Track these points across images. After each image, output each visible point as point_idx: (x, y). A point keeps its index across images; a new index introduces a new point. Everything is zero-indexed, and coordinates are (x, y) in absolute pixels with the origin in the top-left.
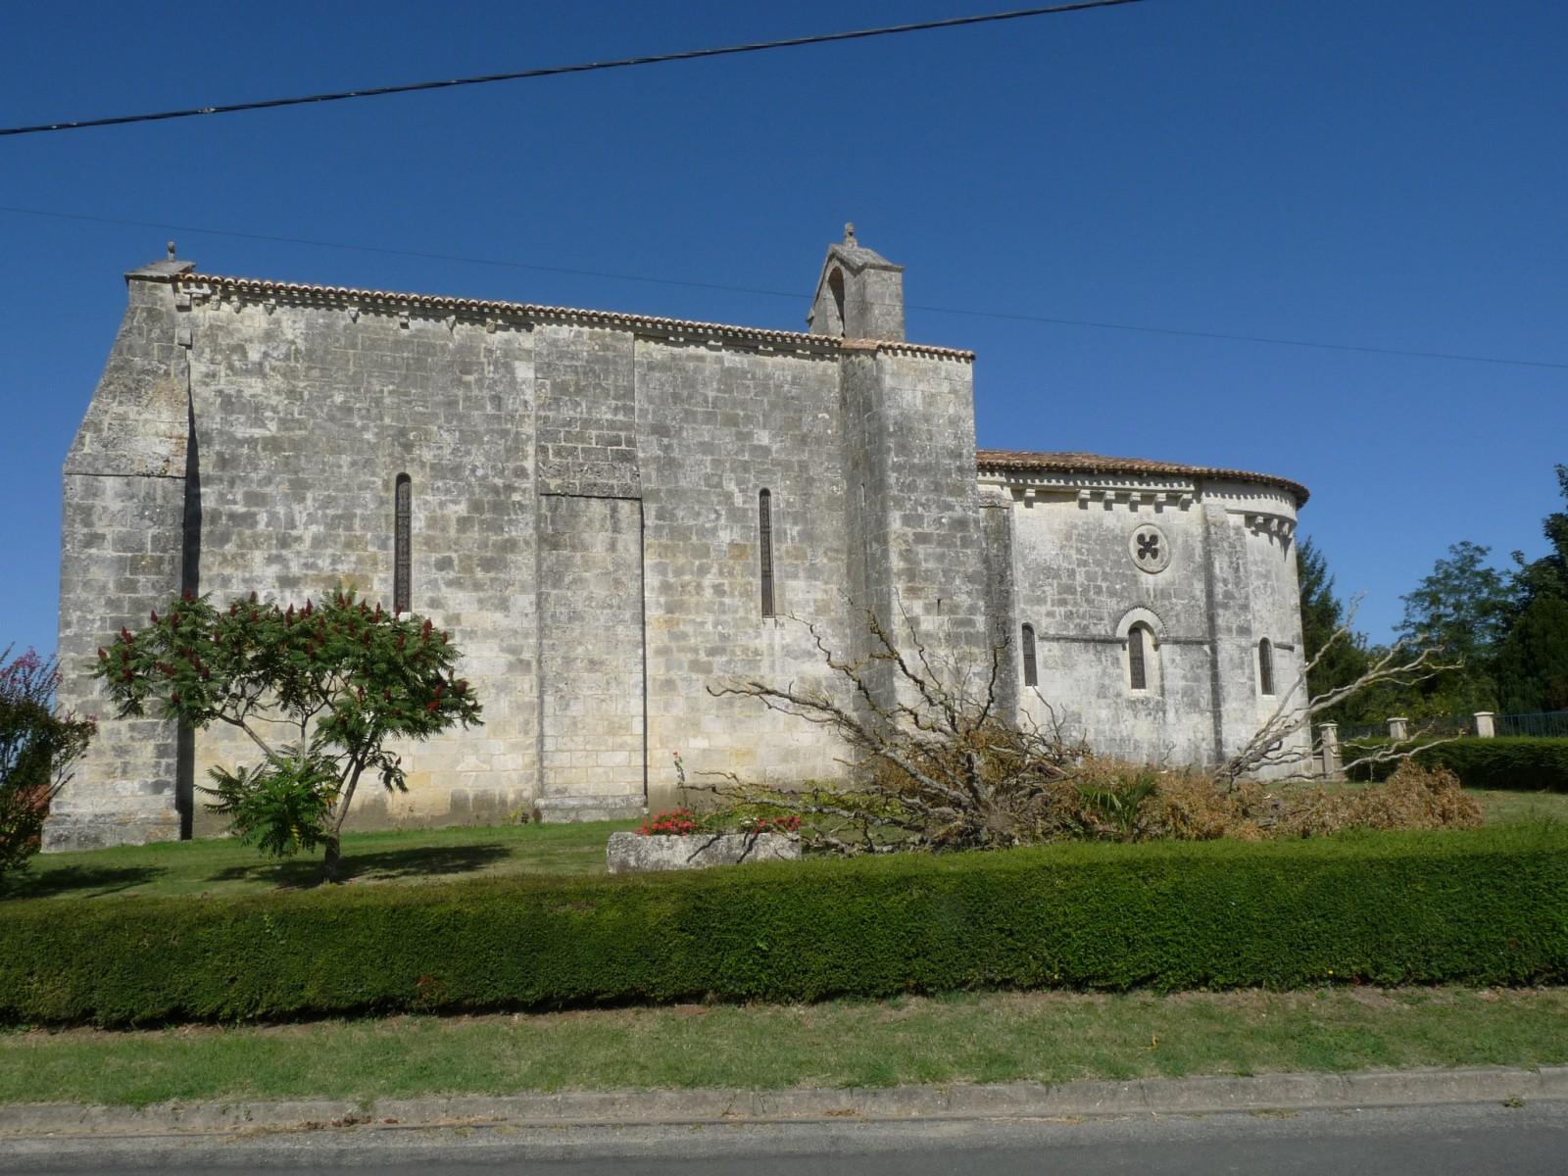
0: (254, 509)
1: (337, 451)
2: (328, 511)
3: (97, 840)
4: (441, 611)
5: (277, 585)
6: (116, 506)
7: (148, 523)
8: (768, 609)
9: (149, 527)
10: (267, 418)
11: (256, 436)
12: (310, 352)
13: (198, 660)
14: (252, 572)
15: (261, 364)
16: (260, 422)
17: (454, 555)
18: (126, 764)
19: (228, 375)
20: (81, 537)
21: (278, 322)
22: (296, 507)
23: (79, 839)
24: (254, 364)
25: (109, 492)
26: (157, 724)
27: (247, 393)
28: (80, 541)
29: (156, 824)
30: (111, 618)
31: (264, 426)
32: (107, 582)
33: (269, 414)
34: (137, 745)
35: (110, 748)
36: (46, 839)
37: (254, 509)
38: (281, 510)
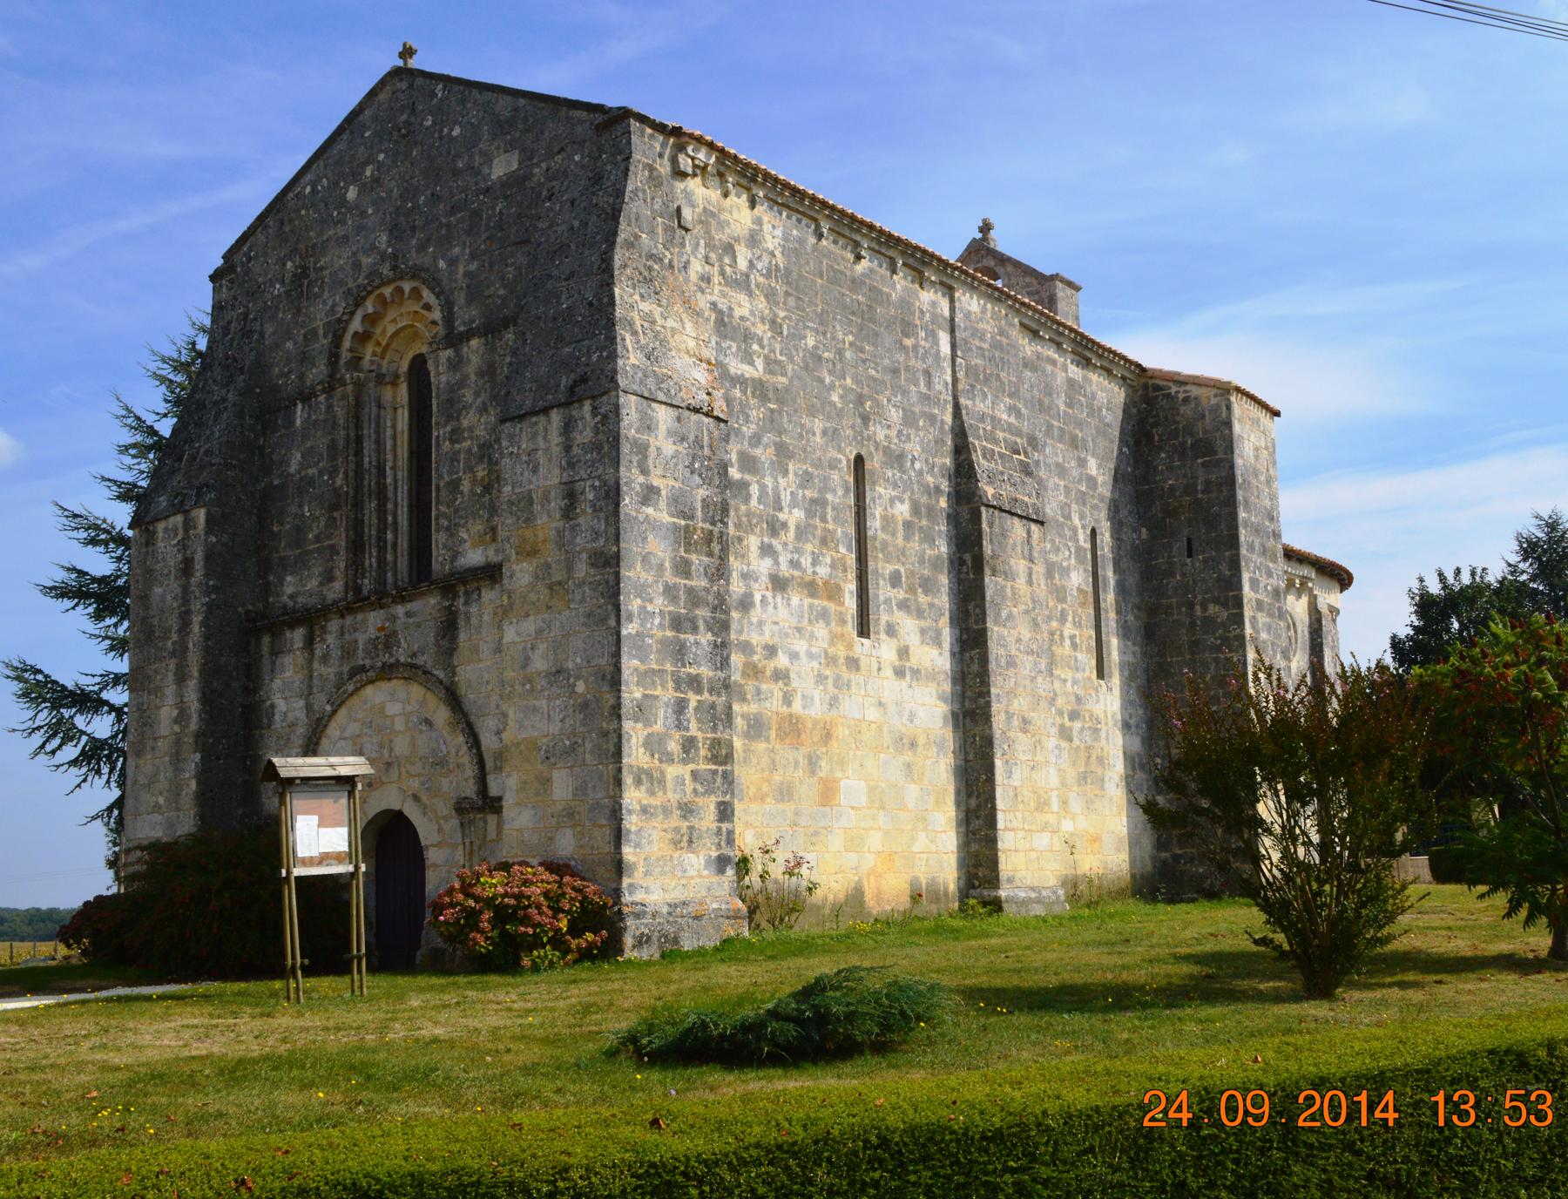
0: (747, 477)
1: (812, 412)
2: (807, 492)
3: (676, 941)
4: (895, 640)
5: (770, 586)
6: (669, 448)
7: (697, 479)
8: (864, 630)
9: (699, 486)
10: (754, 353)
11: (747, 375)
12: (788, 271)
13: (1323, 861)
14: (749, 565)
15: (747, 276)
16: (748, 358)
17: (902, 570)
18: (691, 828)
19: (720, 284)
20: (638, 488)
21: (759, 222)
22: (782, 482)
23: (659, 940)
24: (742, 274)
25: (662, 429)
26: (717, 771)
27: (738, 312)
28: (637, 493)
29: (728, 918)
30: (670, 612)
31: (752, 363)
32: (663, 560)
33: (755, 347)
34: (700, 801)
35: (675, 805)
36: (629, 941)
37: (747, 477)
38: (768, 481)
